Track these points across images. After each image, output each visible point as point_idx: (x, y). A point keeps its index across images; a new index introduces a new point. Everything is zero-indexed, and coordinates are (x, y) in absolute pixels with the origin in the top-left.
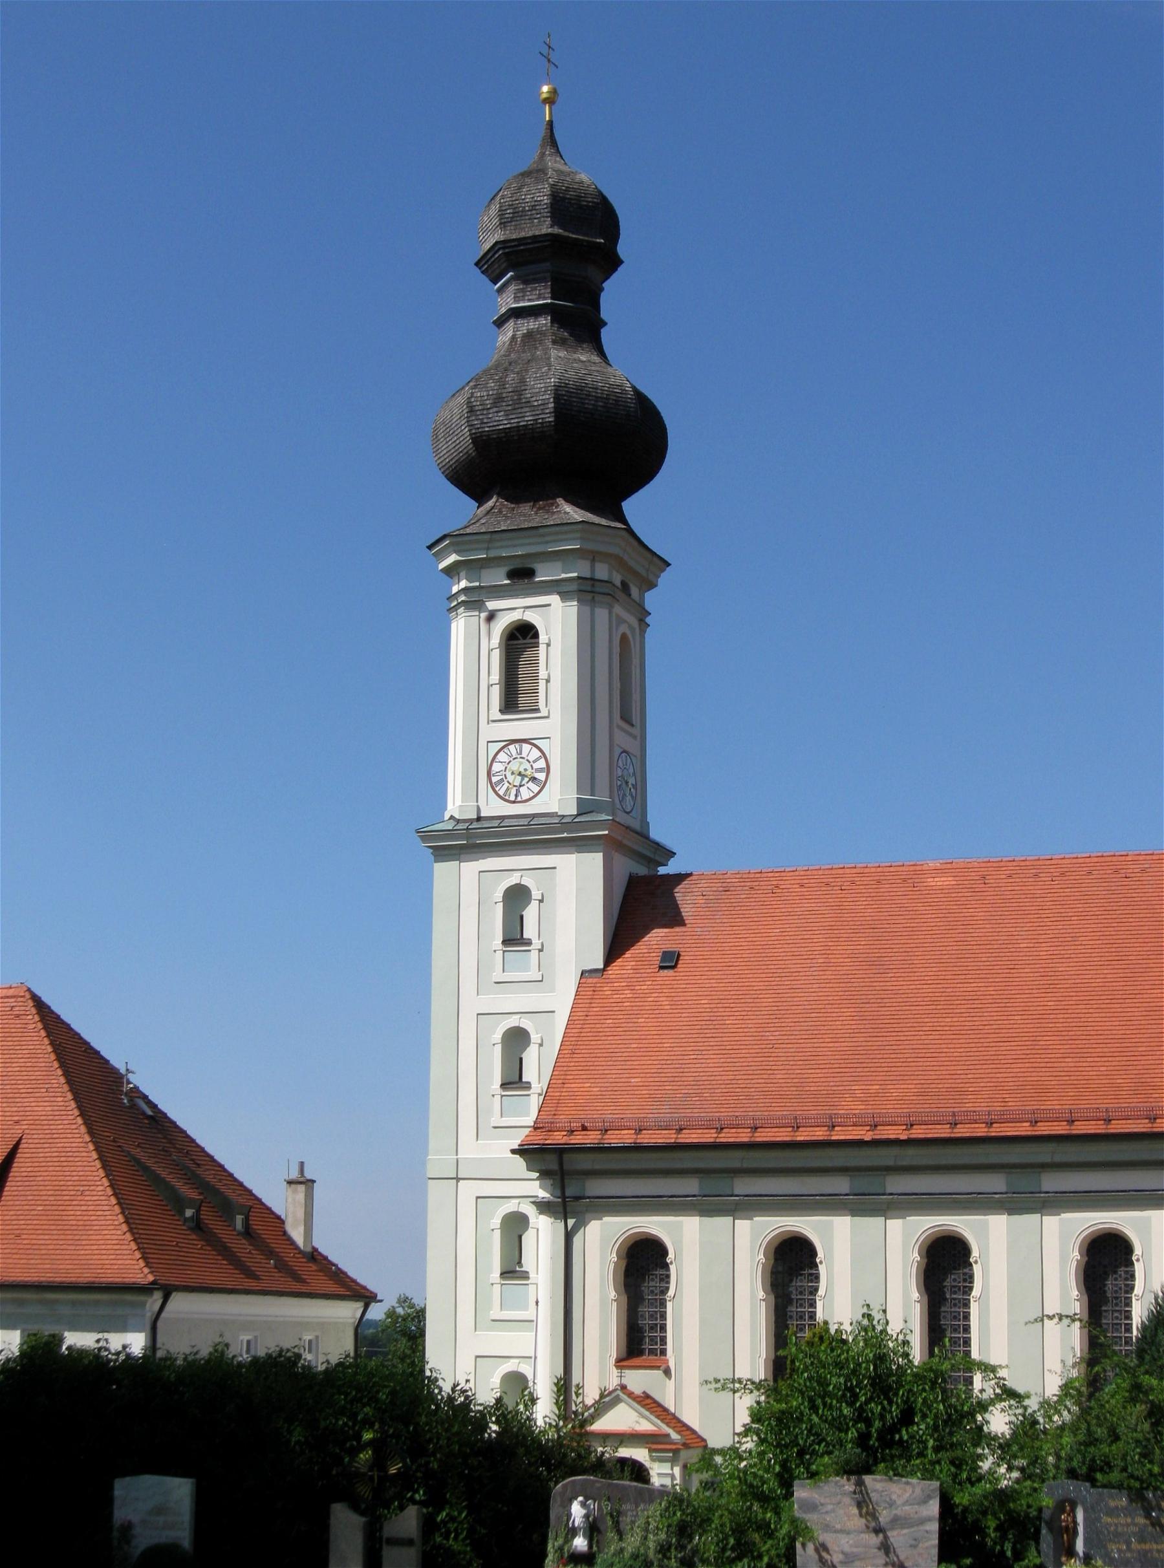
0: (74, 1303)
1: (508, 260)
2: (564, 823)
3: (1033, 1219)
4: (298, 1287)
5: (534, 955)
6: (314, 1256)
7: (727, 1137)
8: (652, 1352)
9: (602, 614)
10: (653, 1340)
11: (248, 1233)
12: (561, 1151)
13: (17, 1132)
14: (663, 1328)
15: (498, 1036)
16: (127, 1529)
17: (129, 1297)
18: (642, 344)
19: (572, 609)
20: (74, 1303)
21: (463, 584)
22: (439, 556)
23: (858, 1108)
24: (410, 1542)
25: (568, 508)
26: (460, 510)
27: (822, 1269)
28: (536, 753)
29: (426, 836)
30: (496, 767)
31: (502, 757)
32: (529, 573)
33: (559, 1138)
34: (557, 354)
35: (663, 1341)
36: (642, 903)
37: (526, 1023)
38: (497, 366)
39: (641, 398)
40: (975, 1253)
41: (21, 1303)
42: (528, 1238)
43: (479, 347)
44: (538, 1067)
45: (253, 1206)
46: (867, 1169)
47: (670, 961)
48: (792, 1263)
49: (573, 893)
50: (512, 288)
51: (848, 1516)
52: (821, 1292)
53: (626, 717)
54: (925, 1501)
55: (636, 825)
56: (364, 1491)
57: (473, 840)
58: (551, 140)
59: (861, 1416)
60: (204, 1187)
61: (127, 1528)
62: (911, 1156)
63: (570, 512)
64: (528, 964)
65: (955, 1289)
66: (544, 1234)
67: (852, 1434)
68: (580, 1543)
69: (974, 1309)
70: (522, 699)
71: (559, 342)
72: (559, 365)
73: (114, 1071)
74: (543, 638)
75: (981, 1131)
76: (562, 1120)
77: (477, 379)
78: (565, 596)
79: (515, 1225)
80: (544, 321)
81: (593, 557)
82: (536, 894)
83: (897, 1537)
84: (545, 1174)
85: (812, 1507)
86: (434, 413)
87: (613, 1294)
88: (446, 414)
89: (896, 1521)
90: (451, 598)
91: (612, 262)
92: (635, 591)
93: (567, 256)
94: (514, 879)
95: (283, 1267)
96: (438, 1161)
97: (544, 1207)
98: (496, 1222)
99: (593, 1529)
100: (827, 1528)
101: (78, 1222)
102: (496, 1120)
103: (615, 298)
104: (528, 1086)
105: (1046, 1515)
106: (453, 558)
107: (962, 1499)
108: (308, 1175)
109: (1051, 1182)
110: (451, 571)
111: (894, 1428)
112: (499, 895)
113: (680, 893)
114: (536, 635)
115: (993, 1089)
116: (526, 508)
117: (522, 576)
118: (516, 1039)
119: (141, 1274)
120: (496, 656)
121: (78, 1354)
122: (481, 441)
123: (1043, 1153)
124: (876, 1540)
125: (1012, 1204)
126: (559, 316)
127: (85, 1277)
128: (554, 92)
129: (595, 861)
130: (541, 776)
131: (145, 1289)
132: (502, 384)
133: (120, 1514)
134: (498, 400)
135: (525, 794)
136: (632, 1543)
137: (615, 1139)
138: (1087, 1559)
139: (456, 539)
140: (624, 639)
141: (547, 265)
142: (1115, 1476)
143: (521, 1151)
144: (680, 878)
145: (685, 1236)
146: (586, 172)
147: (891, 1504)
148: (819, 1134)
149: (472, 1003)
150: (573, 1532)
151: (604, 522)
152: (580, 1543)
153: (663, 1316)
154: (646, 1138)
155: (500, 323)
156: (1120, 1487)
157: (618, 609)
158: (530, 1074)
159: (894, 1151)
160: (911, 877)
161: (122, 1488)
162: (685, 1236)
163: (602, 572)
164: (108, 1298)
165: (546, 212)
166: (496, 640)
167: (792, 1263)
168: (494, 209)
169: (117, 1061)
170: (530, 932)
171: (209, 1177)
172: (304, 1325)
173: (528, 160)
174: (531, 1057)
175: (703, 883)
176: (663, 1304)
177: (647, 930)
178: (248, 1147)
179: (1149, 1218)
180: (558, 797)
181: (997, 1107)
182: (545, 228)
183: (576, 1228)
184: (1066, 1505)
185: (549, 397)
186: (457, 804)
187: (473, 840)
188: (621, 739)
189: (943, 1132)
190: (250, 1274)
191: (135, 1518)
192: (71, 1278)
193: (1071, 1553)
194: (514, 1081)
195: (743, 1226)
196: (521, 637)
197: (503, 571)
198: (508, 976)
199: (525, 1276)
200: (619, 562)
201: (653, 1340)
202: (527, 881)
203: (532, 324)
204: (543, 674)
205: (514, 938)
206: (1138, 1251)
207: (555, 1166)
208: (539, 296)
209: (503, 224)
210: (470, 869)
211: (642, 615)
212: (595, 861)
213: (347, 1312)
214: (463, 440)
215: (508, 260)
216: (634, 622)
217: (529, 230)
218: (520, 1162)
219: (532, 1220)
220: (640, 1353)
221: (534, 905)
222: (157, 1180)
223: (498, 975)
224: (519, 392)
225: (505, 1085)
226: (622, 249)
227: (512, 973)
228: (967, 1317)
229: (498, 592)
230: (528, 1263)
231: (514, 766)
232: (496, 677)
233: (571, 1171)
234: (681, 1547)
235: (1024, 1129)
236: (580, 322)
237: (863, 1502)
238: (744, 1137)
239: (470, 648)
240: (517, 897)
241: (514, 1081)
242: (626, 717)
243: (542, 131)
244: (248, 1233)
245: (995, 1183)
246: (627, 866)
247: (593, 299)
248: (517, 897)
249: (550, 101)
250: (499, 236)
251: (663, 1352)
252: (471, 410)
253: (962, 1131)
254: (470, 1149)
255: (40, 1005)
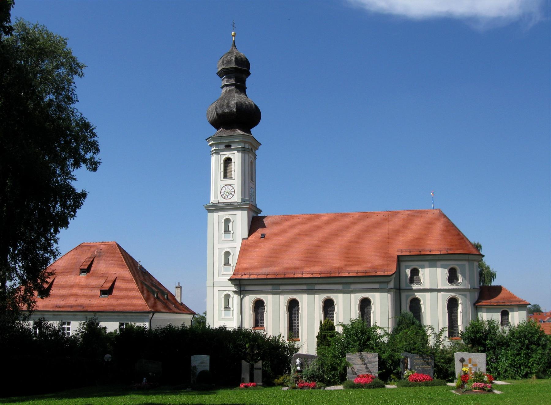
0: (131, 316)
1: (225, 73)
2: (238, 204)
3: (277, 296)
4: (180, 311)
5: (231, 234)
6: (182, 304)
7: (278, 277)
8: (261, 326)
9: (247, 156)
10: (261, 323)
11: (168, 299)
12: (240, 280)
13: (115, 276)
14: (263, 320)
15: (223, 253)
16: (195, 367)
17: (145, 314)
18: (255, 93)
19: (240, 154)
20: (131, 316)
21: (214, 148)
22: (208, 142)
23: (337, 269)
24: (260, 369)
25: (239, 131)
26: (213, 131)
27: (266, 307)
28: (232, 188)
29: (206, 207)
30: (222, 191)
31: (224, 188)
32: (230, 146)
33: (239, 277)
34: (236, 95)
35: (263, 323)
36: (256, 223)
37: (229, 250)
38: (222, 98)
39: (255, 105)
40: (335, 303)
41: (119, 316)
42: (230, 300)
43: (218, 94)
44: (233, 260)
45: (169, 293)
46: (347, 282)
47: (263, 236)
48: (328, 305)
49: (240, 220)
50: (225, 79)
51: (359, 361)
52: (300, 312)
53: (252, 180)
54: (375, 357)
55: (254, 204)
56: (249, 358)
57: (217, 208)
58: (234, 45)
59: (359, 339)
60: (157, 288)
61: (195, 367)
62: (321, 281)
63: (239, 132)
64: (230, 237)
65: (330, 311)
66: (235, 300)
67: (358, 343)
68: (299, 368)
69: (299, 315)
70: (228, 176)
71: (237, 92)
72: (236, 98)
73: (136, 262)
74: (233, 161)
75: (337, 275)
76: (240, 273)
77: (218, 100)
78: (238, 151)
79: (227, 297)
80: (233, 87)
81: (245, 142)
82: (232, 220)
83: (369, 365)
84: (236, 285)
85: (350, 359)
86: (209, 108)
87: (252, 313)
88: (209, 109)
89: (369, 362)
90: (211, 151)
91: (248, 74)
92: (253, 150)
93: (238, 72)
94: (227, 217)
95: (176, 307)
96: (209, 282)
97: (235, 293)
98: (223, 296)
99: (301, 365)
100: (354, 364)
101: (131, 297)
102: (223, 273)
103: (249, 82)
104: (230, 265)
105: (401, 360)
106: (212, 142)
107: (384, 356)
108: (180, 285)
109: (353, 287)
110: (211, 145)
111: (366, 342)
112: (223, 220)
113: (265, 220)
114: (232, 160)
115: (339, 265)
116: (229, 131)
117: (228, 147)
118: (227, 254)
119: (148, 309)
120: (222, 165)
121: (139, 327)
122: (219, 116)
123: (351, 280)
124: (364, 366)
125: (344, 292)
126: (237, 86)
127: (135, 310)
128: (235, 34)
129: (245, 213)
130: (233, 193)
131: (149, 312)
132: (224, 102)
133: (193, 364)
134: (223, 106)
135: (229, 197)
136: (311, 368)
137: (252, 277)
138: (410, 369)
139: (213, 138)
140: (251, 162)
141: (234, 74)
142: (416, 351)
143: (230, 280)
144: (265, 217)
145: (269, 299)
146: (243, 53)
147: (368, 358)
148: (300, 276)
149: (217, 246)
150: (297, 366)
151: (245, 134)
152: (299, 368)
153: (263, 317)
154: (260, 277)
155: (222, 87)
156: (418, 354)
157: (250, 155)
158: (230, 262)
159: (317, 280)
160: (318, 217)
161: (193, 358)
162: (269, 299)
163: (247, 146)
164: (140, 314)
165: (234, 62)
166: (222, 162)
167: (328, 305)
168: (221, 61)
169: (137, 259)
170: (230, 229)
171: (158, 286)
172: (180, 320)
173: (229, 50)
174: (231, 258)
175: (270, 218)
176: (263, 315)
177: (257, 229)
178: (167, 280)
179: (425, 295)
180: (237, 198)
181: (340, 270)
182: (234, 66)
183: (243, 297)
184: (406, 358)
185: (235, 105)
186: (213, 199)
187: (217, 208)
188: (251, 185)
189: (328, 275)
190: (170, 309)
191: (196, 365)
192: (131, 310)
193: (407, 368)
194: (227, 263)
195: (282, 297)
196: (228, 161)
197: (224, 145)
198: (225, 239)
199: (230, 308)
200: (251, 144)
201: (261, 323)
202: (230, 217)
203: (229, 88)
204: (233, 169)
205: (227, 231)
206: (300, 303)
207: (238, 283)
208: (232, 81)
209: (223, 65)
210: (216, 215)
211: (255, 156)
212: (245, 213)
213: (190, 317)
214: (214, 115)
215: (225, 73)
216: (253, 157)
217: (229, 66)
218: (230, 282)
219: (232, 296)
220: (258, 326)
221: (231, 223)
222: (148, 287)
223: (223, 239)
224: (228, 104)
225: (225, 265)
226: (250, 71)
227: (226, 239)
228: (333, 317)
229: (223, 150)
230: (230, 305)
231: (227, 191)
232: (222, 170)
233: (241, 284)
234: (322, 369)
235: (347, 275)
236: (241, 88)
237: (362, 358)
238: (282, 276)
239: (216, 162)
240: (227, 221)
241: (227, 263)
242: (252, 180)
243: (232, 43)
244: (168, 299)
245: (340, 287)
246: (253, 214)
247: (244, 82)
248: (227, 221)
249: (234, 36)
250: (222, 67)
251: (263, 326)
252: (217, 108)
253: (332, 275)
254: (217, 279)
255: (118, 245)
